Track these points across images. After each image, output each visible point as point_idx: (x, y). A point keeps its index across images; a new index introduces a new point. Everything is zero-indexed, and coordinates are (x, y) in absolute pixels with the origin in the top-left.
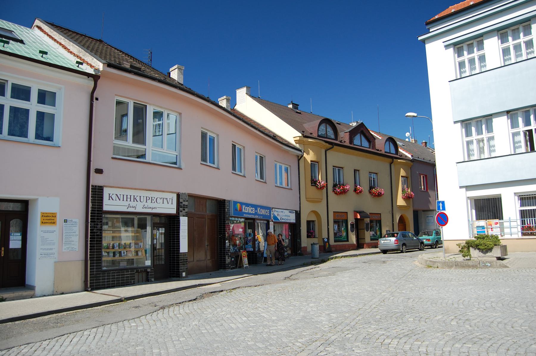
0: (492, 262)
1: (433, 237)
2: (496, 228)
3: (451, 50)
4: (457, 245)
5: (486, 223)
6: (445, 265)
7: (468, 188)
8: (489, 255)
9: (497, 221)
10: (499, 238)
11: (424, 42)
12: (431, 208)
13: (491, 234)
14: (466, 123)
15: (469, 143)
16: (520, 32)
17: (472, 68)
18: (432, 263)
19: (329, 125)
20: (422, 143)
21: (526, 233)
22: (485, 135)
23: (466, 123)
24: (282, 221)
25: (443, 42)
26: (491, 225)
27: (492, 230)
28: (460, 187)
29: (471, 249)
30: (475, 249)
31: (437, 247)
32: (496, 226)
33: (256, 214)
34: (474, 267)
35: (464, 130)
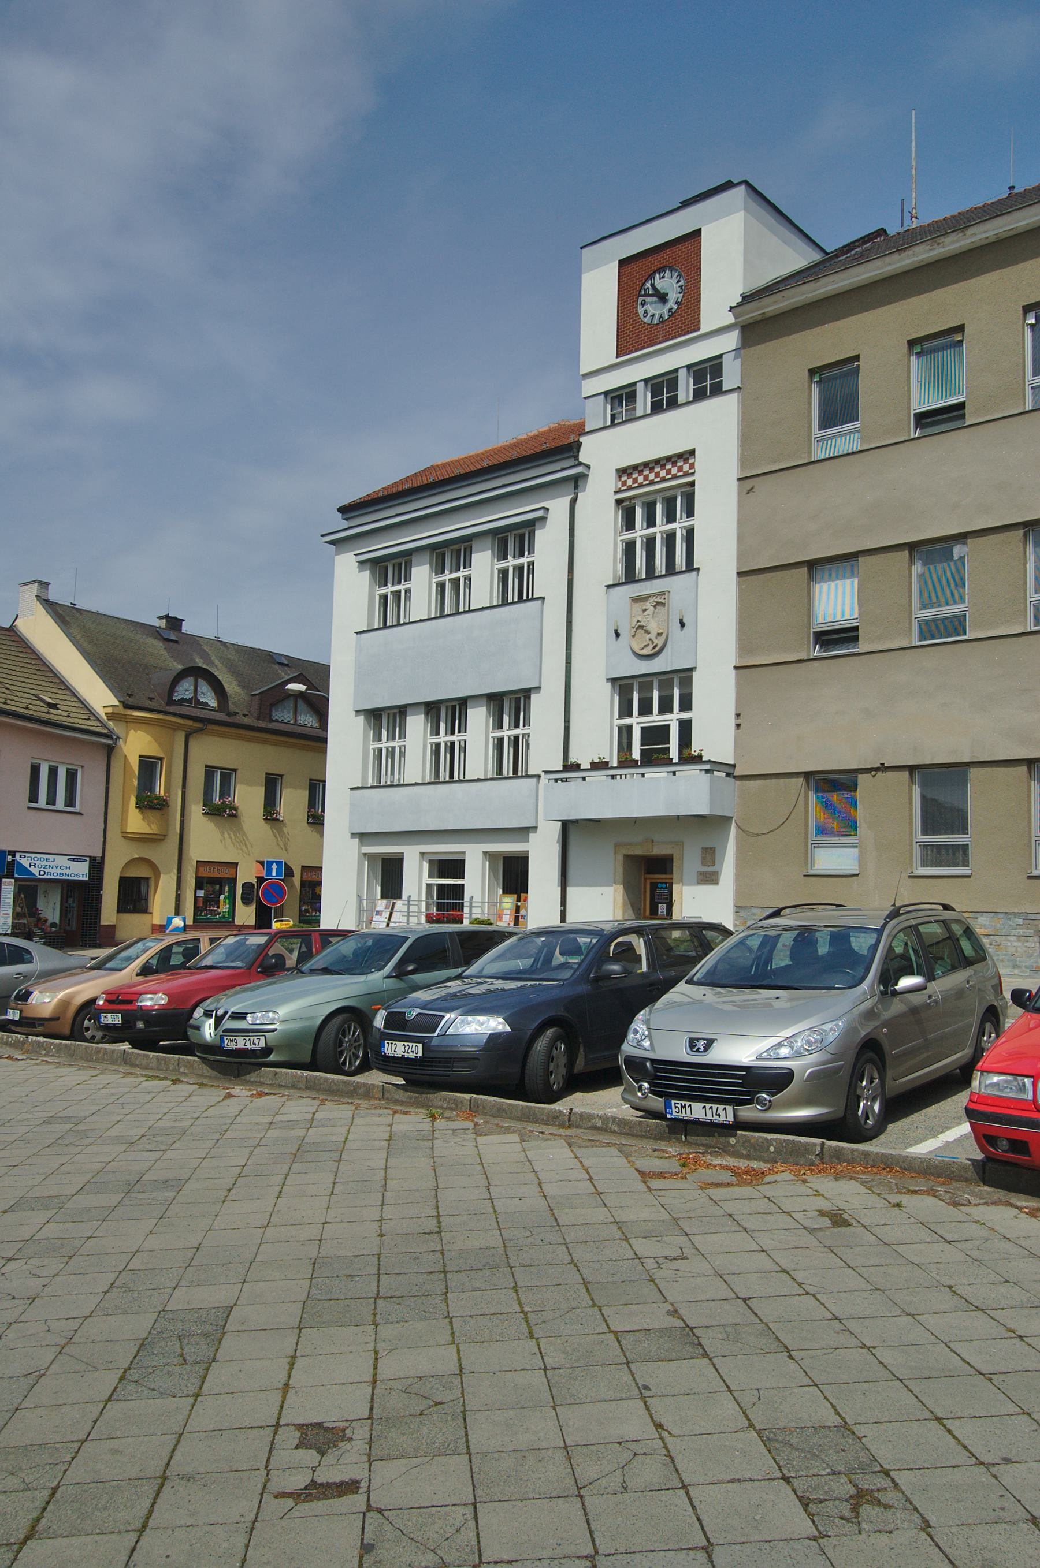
14: (375, 716)
19: (205, 679)
23: (375, 716)
24: (45, 877)
28: (352, 834)
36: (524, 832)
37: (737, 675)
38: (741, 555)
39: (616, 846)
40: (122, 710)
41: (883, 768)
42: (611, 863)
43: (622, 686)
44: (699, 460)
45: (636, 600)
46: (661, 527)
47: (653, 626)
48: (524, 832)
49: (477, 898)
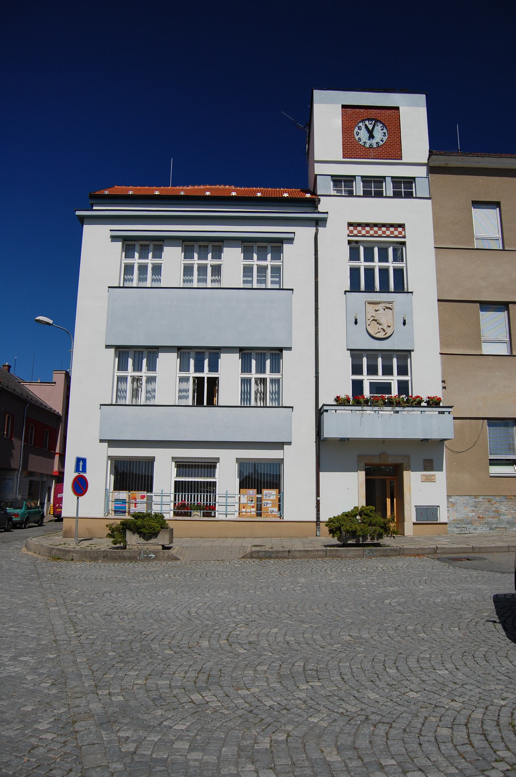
0: (158, 552)
1: (23, 510)
2: (141, 503)
3: (119, 245)
4: (107, 526)
5: (129, 495)
6: (86, 557)
7: (113, 443)
8: (152, 542)
9: (144, 493)
10: (165, 518)
11: (82, 220)
12: (13, 466)
13: (133, 511)
15: (122, 379)
16: (268, 253)
17: (142, 277)
18: (63, 553)
20: (4, 366)
21: (179, 512)
22: (144, 373)
25: (111, 230)
26: (135, 499)
27: (135, 506)
29: (128, 534)
30: (134, 534)
31: (27, 526)
32: (142, 500)
34: (132, 559)
35: (117, 359)
37: (441, 357)
38: (440, 290)
39: (359, 456)
46: (377, 264)
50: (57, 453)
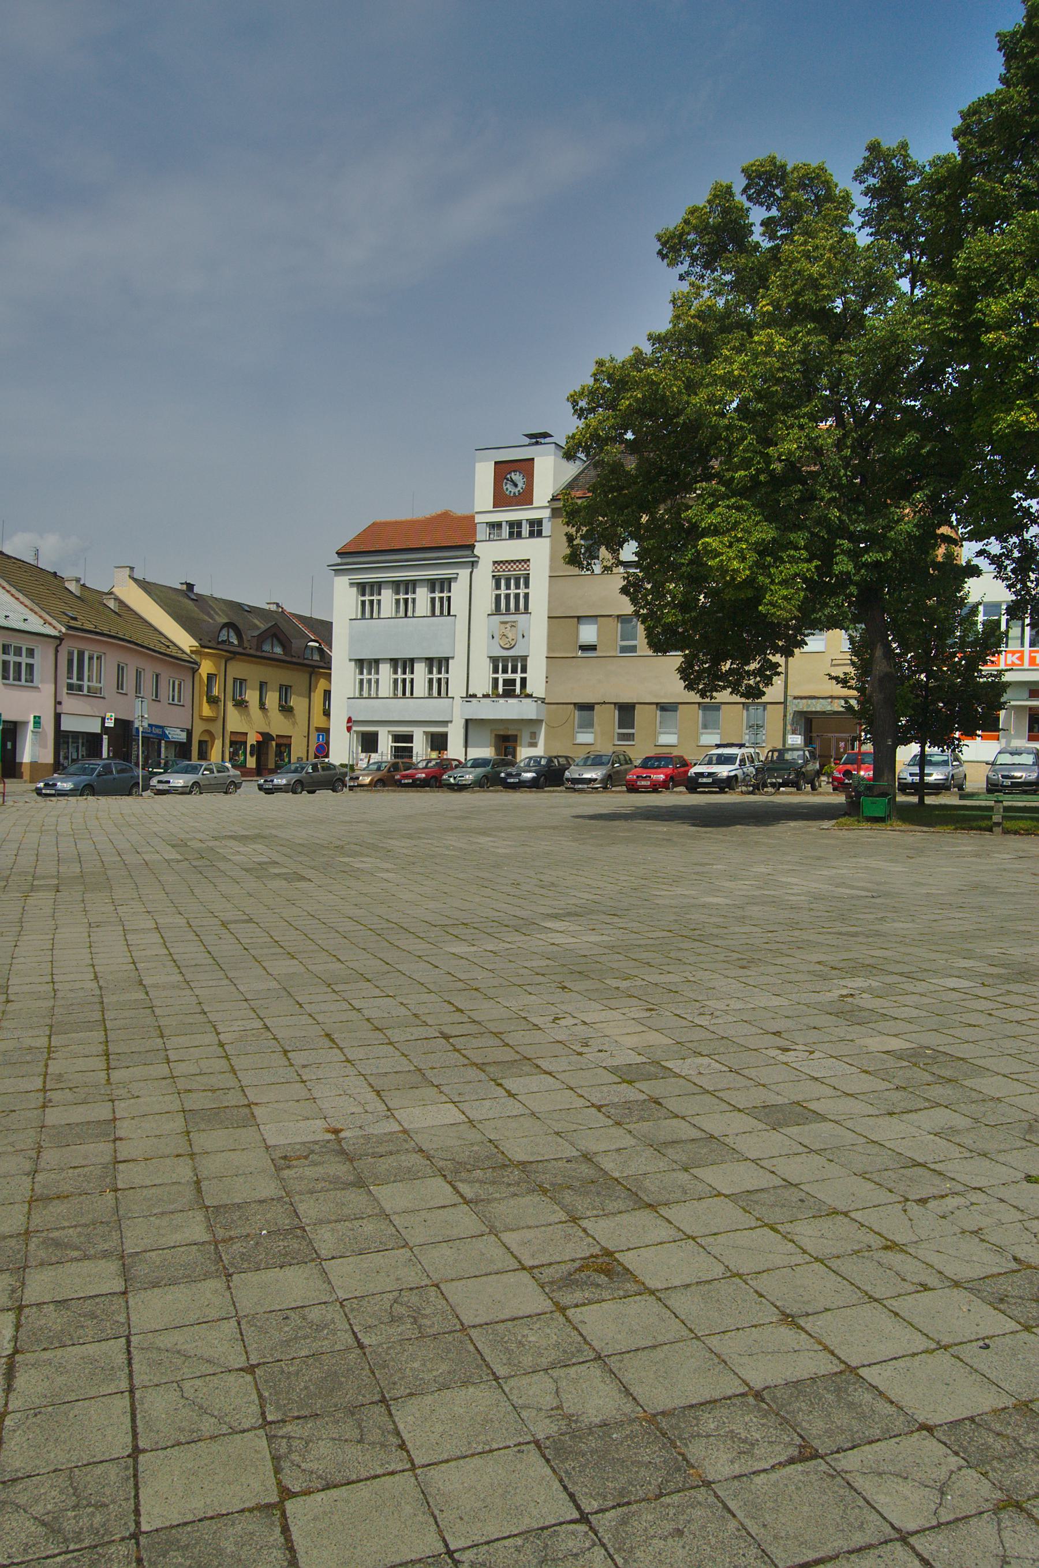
14: (360, 663)
23: (360, 663)
33: (151, 733)
36: (446, 723)
38: (549, 610)
40: (200, 649)
41: (604, 703)
42: (488, 736)
43: (494, 660)
44: (532, 564)
45: (502, 623)
46: (513, 591)
47: (510, 635)
48: (446, 723)
49: (420, 752)
50: (921, 800)
